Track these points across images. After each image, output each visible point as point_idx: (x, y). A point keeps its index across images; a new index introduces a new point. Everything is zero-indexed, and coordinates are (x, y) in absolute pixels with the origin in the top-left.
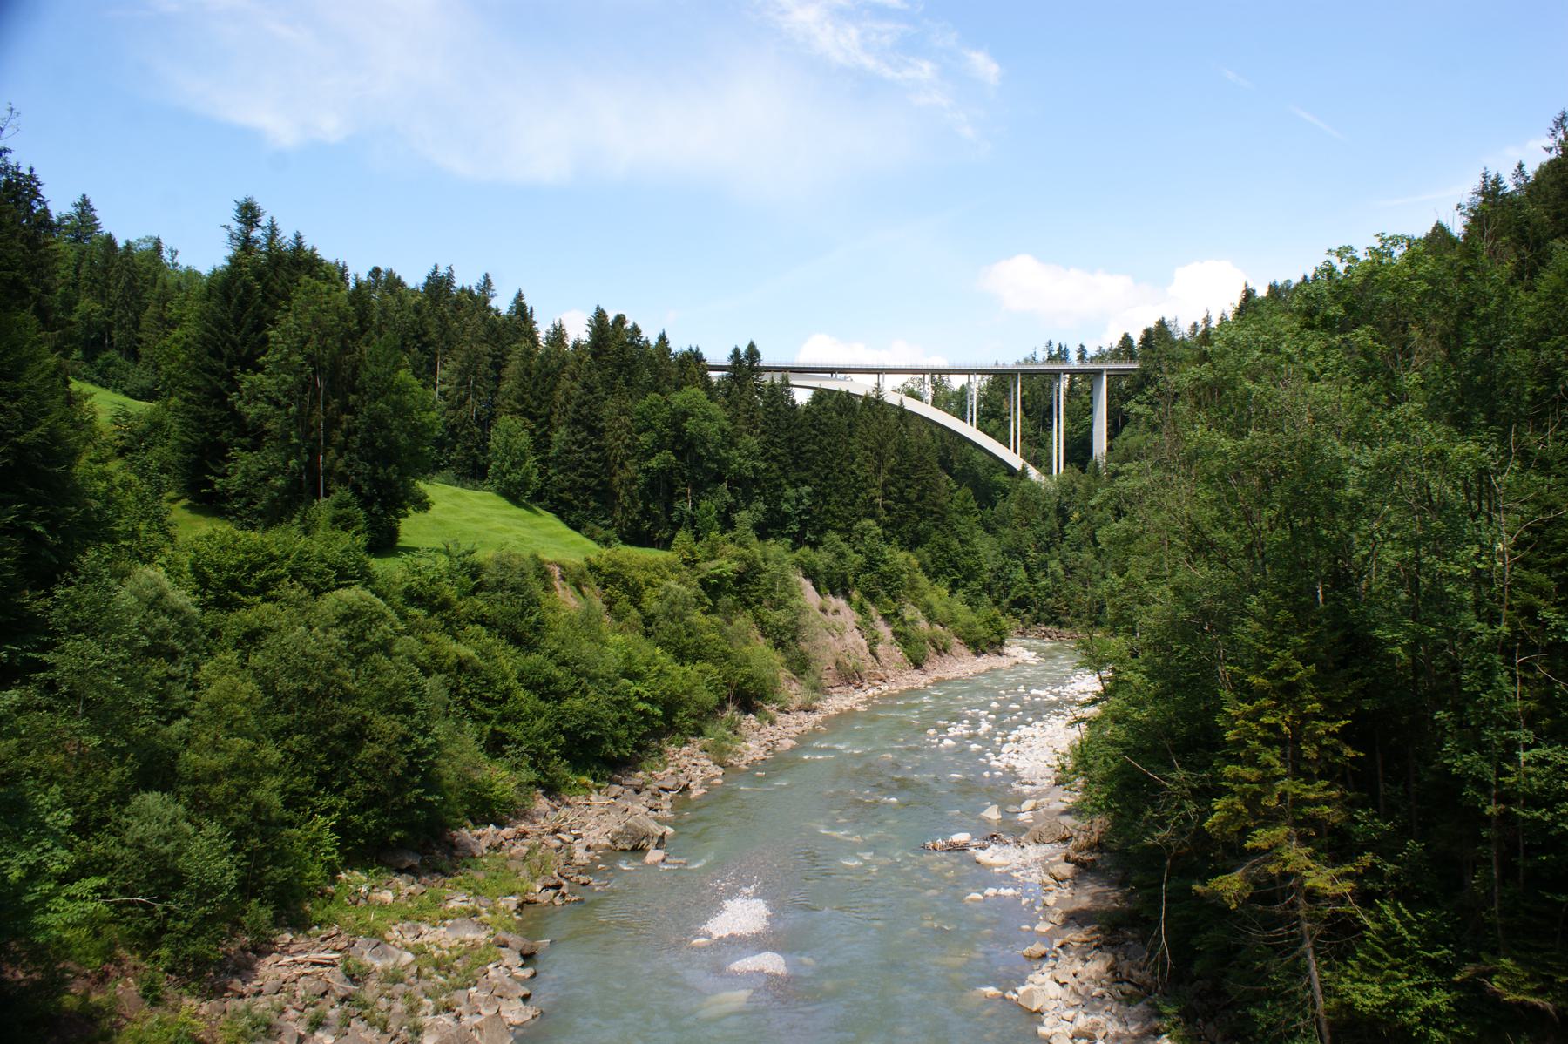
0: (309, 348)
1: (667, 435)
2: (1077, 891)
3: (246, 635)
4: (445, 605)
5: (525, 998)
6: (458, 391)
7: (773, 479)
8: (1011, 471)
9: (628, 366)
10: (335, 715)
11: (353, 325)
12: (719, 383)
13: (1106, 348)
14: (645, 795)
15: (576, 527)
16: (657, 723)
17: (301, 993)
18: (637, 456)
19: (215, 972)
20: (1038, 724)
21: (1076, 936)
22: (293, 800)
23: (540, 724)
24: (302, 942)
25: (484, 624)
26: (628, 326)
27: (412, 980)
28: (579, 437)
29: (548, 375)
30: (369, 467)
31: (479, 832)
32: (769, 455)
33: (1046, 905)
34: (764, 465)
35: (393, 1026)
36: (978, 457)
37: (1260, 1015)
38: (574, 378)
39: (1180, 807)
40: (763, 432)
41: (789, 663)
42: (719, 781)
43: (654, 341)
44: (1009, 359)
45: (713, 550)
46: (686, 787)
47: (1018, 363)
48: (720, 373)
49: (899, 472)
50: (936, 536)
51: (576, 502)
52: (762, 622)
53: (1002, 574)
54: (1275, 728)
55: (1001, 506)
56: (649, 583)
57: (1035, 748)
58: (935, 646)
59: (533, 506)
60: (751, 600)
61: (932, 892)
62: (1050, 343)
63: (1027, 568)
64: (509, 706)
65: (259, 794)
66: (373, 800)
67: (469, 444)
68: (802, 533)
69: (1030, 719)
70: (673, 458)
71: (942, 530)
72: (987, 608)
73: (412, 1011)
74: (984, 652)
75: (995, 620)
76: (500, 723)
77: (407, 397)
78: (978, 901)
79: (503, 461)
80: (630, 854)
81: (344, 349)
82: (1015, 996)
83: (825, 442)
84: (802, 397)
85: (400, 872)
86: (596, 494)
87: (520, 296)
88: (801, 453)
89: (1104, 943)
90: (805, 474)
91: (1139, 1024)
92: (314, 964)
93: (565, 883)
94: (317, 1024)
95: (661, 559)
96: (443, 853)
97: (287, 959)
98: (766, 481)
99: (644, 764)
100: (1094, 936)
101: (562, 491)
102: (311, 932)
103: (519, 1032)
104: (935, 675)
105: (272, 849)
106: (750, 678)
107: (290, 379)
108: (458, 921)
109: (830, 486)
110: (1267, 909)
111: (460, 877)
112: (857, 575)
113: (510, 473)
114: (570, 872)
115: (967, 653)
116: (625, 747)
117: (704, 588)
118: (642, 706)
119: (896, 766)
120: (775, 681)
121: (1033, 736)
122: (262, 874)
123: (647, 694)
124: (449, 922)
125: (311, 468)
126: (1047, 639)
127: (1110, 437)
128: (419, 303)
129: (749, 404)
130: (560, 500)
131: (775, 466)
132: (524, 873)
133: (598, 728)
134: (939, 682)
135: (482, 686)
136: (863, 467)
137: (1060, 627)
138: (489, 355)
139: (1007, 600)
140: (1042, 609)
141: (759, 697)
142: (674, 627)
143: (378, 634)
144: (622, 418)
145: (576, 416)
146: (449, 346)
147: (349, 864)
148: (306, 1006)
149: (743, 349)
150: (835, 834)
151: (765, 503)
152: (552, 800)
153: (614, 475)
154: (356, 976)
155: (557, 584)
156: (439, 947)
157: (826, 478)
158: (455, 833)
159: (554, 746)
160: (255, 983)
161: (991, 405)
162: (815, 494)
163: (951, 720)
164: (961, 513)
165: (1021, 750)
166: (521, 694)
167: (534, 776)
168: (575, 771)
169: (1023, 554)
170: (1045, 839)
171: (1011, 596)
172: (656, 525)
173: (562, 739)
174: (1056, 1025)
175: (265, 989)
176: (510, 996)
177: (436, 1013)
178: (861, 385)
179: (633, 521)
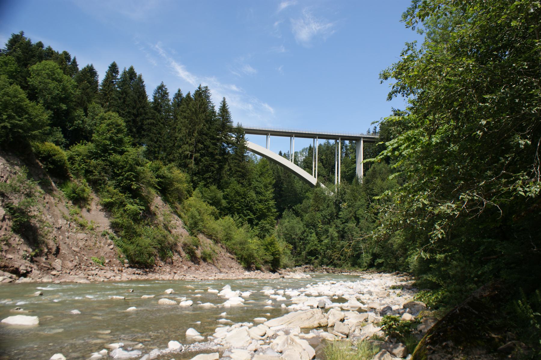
63: (317, 234)
127: (364, 172)
137: (335, 267)
140: (324, 257)
169: (315, 226)
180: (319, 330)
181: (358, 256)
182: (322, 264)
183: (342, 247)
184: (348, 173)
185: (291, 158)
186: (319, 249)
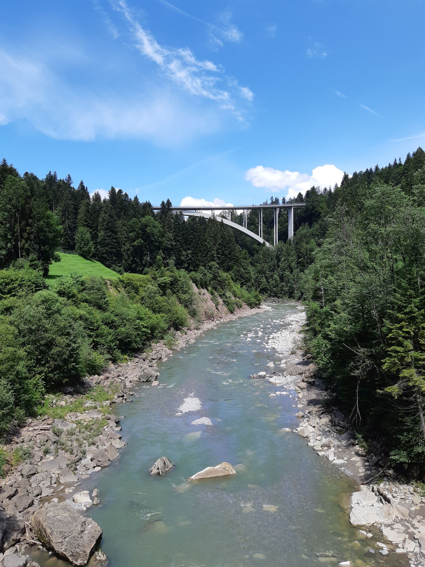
0: (13, 202)
1: (140, 233)
2: (310, 392)
3: (5, 309)
4: (74, 296)
5: (120, 438)
6: (62, 218)
7: (178, 248)
8: (259, 243)
9: (124, 208)
10: (42, 337)
11: (29, 194)
13: (292, 198)
14: (147, 361)
15: (109, 267)
17: (38, 441)
18: (130, 241)
19: (7, 435)
20: (279, 332)
21: (314, 409)
22: (30, 369)
23: (110, 338)
24: (35, 422)
25: (87, 302)
26: (124, 193)
27: (78, 434)
28: (109, 234)
29: (95, 212)
30: (38, 246)
31: (91, 378)
34: (174, 243)
35: (75, 451)
36: (248, 239)
37: (402, 438)
38: (105, 213)
39: (364, 362)
40: (174, 232)
41: (189, 312)
42: (172, 355)
43: (133, 199)
44: (258, 203)
45: (162, 273)
46: (161, 358)
47: (261, 205)
49: (222, 245)
50: (235, 267)
51: (108, 258)
52: (180, 298)
53: (257, 280)
54: (408, 333)
55: (256, 256)
56: (141, 286)
57: (281, 341)
58: (237, 306)
59: (92, 259)
60: (175, 291)
62: (272, 197)
63: (266, 278)
64: (99, 331)
65: (19, 368)
66: (57, 368)
67: (67, 237)
69: (276, 331)
70: (143, 241)
71: (237, 265)
72: (254, 293)
73: (80, 445)
74: (253, 307)
75: (257, 296)
76: (96, 337)
77: (51, 220)
79: (81, 243)
80: (145, 384)
81: (26, 203)
82: (297, 432)
84: (186, 218)
85: (66, 394)
86: (116, 255)
87: (82, 183)
88: (187, 239)
89: (325, 412)
90: (189, 246)
92: (41, 430)
93: (125, 395)
94: (47, 452)
95: (144, 277)
96: (80, 386)
97: (31, 429)
99: (145, 350)
100: (321, 409)
101: (103, 254)
102: (38, 418)
104: (238, 315)
105: (23, 388)
106: (178, 318)
107: (7, 214)
108: (90, 411)
109: (198, 250)
110: (408, 399)
111: (88, 395)
112: (210, 281)
113: (84, 248)
114: (126, 390)
115: (248, 308)
116: (139, 344)
118: (144, 329)
119: (232, 348)
121: (278, 337)
122: (20, 397)
123: (145, 325)
124: (87, 412)
125: (15, 247)
127: (294, 231)
128: (45, 186)
129: (169, 221)
130: (102, 257)
131: (178, 244)
132: (110, 392)
133: (129, 338)
134: (240, 318)
135: (89, 324)
136: (209, 243)
138: (73, 205)
139: (259, 289)
141: (181, 325)
142: (151, 301)
143: (56, 307)
144: (124, 227)
146: (58, 202)
147: (48, 392)
148: (42, 445)
149: (165, 202)
150: (217, 373)
152: (115, 365)
153: (122, 248)
154: (57, 434)
156: (85, 421)
157: (196, 248)
158: (84, 379)
159: (115, 345)
160: (21, 438)
161: (251, 220)
162: (193, 253)
163: (248, 332)
164: (244, 259)
165: (276, 342)
166: (104, 327)
167: (109, 356)
168: (122, 354)
169: (264, 273)
170: (293, 373)
172: (137, 266)
173: (118, 342)
175: (25, 440)
177: (89, 446)
178: (207, 214)
179: (129, 264)
180: (28, 470)
182: (270, 296)
183: (283, 286)
185: (244, 223)
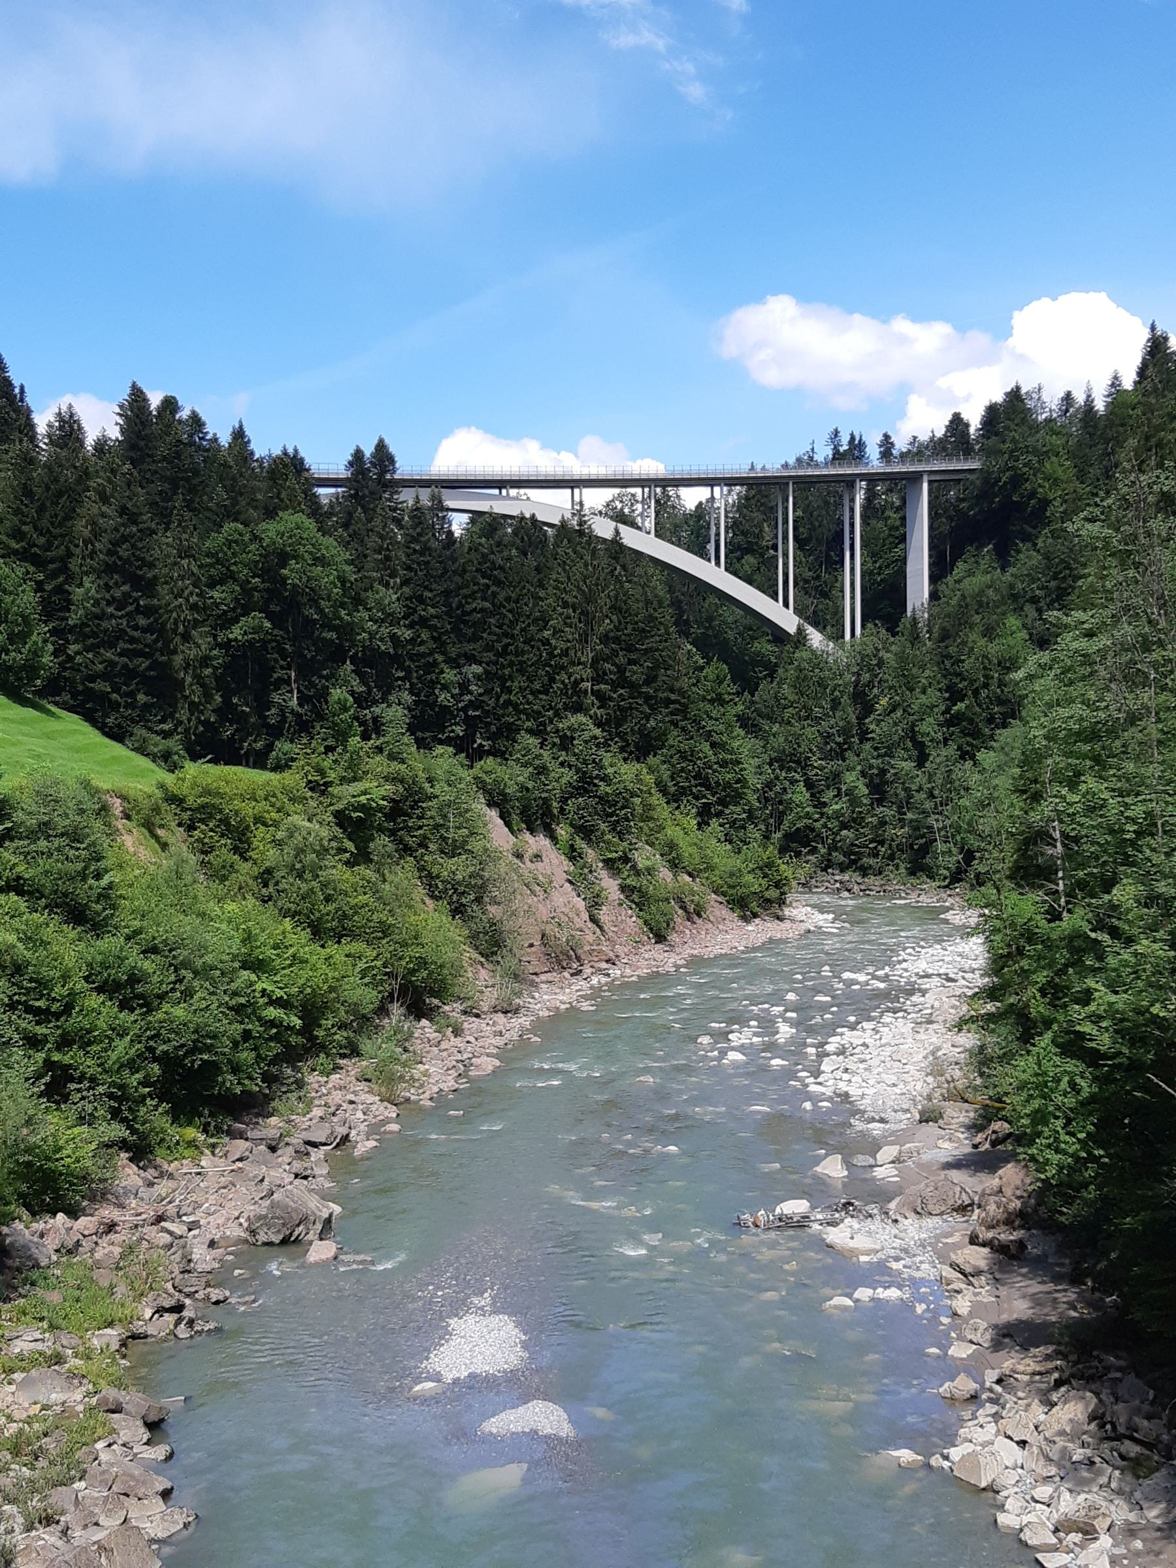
1: (255, 589)
2: (1003, 1291)
5: (166, 1494)
7: (423, 655)
8: (778, 635)
9: (187, 479)
12: (331, 505)
13: (924, 437)
14: (286, 1154)
15: (117, 735)
16: (294, 1040)
23: (122, 1048)
25: (20, 893)
26: (184, 414)
28: (118, 594)
29: (60, 494)
31: (39, 1226)
32: (416, 618)
33: (955, 1314)
34: (408, 634)
36: (729, 615)
38: (104, 498)
40: (405, 582)
42: (395, 1127)
43: (225, 439)
45: (353, 765)
46: (345, 1139)
47: (786, 466)
48: (332, 490)
49: (616, 640)
50: (674, 738)
52: (430, 876)
55: (765, 690)
56: (259, 820)
58: (684, 908)
59: (44, 702)
60: (412, 842)
61: (770, 1295)
62: (836, 433)
63: (809, 785)
64: (75, 1021)
68: (469, 737)
70: (268, 624)
71: (683, 729)
72: (758, 850)
74: (755, 916)
75: (770, 865)
78: (845, 1308)
82: (946, 1464)
83: (502, 596)
84: (458, 524)
86: (147, 684)
88: (464, 613)
89: (1073, 1376)
91: (1163, 1506)
93: (188, 1301)
98: (412, 658)
99: (275, 1104)
101: (92, 678)
103: (167, 1550)
104: (688, 951)
106: (423, 962)
109: (511, 664)
111: (22, 1302)
112: (564, 800)
114: (193, 1283)
115: (731, 918)
116: (251, 1078)
117: (340, 825)
118: (272, 1013)
119: (662, 1095)
120: (458, 971)
121: (865, 1045)
123: (279, 993)
124: (18, 1376)
126: (846, 894)
127: (933, 579)
129: (381, 537)
130: (90, 694)
131: (425, 635)
132: (121, 1290)
133: (209, 1049)
134: (696, 963)
135: (29, 990)
139: (778, 835)
140: (833, 848)
142: (304, 887)
144: (185, 562)
145: (111, 560)
149: (368, 451)
150: (594, 1205)
151: (412, 693)
152: (144, 1169)
153: (175, 652)
155: (120, 824)
157: (504, 652)
162: (488, 676)
163: (731, 1021)
164: (712, 701)
166: (94, 1001)
167: (118, 1131)
169: (803, 764)
170: (930, 1207)
171: (785, 826)
172: (244, 731)
173: (156, 1069)
174: (1025, 1510)
176: (141, 1491)
177: (29, 1528)
179: (206, 723)
181: (925, 849)
182: (828, 867)
183: (883, 823)
184: (879, 574)
185: (711, 547)
186: (818, 825)
